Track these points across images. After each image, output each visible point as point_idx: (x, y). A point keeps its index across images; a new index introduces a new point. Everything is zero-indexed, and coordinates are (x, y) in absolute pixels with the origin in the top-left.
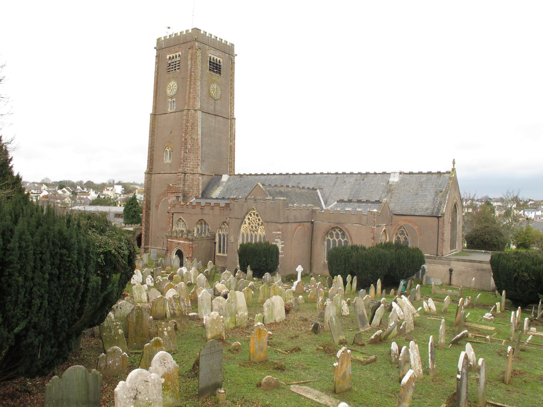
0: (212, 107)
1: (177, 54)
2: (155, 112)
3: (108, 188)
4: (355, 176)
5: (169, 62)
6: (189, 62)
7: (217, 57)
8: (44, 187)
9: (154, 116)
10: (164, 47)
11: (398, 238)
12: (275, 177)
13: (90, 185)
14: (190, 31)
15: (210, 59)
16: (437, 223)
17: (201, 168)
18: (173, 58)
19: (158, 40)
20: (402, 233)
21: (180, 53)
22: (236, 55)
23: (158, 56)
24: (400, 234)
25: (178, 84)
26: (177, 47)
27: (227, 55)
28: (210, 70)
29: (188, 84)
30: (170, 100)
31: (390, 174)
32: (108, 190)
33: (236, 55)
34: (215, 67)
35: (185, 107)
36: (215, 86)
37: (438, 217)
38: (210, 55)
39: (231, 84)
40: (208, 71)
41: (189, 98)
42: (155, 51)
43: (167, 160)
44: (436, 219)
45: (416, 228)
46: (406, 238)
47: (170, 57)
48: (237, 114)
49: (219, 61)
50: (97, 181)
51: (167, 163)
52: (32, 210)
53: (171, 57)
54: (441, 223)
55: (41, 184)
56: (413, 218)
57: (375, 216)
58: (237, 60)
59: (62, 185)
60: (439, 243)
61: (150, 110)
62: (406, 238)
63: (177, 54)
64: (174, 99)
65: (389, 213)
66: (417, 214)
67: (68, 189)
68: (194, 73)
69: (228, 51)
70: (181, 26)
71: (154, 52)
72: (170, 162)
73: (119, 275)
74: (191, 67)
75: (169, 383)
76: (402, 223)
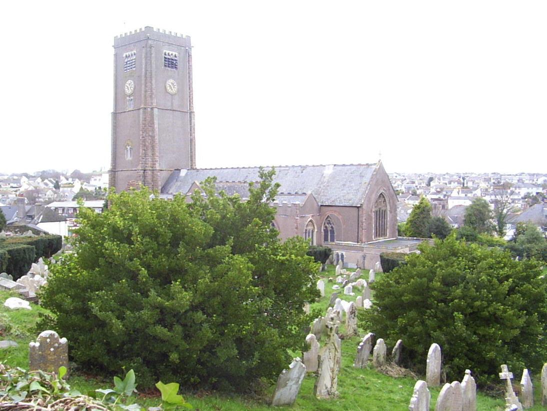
0: (170, 104)
1: (133, 52)
4: (355, 167)
5: (126, 61)
6: (144, 61)
7: (172, 53)
8: (24, 179)
9: (115, 115)
10: (121, 44)
11: (326, 227)
12: (226, 171)
13: (77, 175)
15: (165, 54)
16: (356, 214)
18: (129, 56)
20: (329, 223)
21: (135, 52)
22: (193, 47)
23: (116, 55)
24: (328, 223)
25: (134, 82)
26: (132, 46)
27: (183, 48)
28: (165, 66)
29: (143, 82)
31: (325, 166)
33: (193, 47)
34: (171, 63)
35: (141, 105)
39: (189, 77)
41: (145, 96)
42: (113, 49)
43: (129, 157)
44: (356, 208)
45: (340, 217)
46: (332, 227)
47: (126, 56)
48: (196, 108)
49: (175, 55)
51: (129, 160)
53: (128, 56)
54: (360, 213)
56: (338, 208)
57: (298, 208)
58: (194, 53)
59: (44, 176)
60: (359, 231)
61: (111, 109)
62: (332, 227)
63: (133, 52)
64: (132, 98)
66: (341, 205)
68: (152, 71)
69: (184, 45)
71: (112, 51)
72: (131, 159)
73: (504, 367)
75: (250, 381)
76: (328, 214)
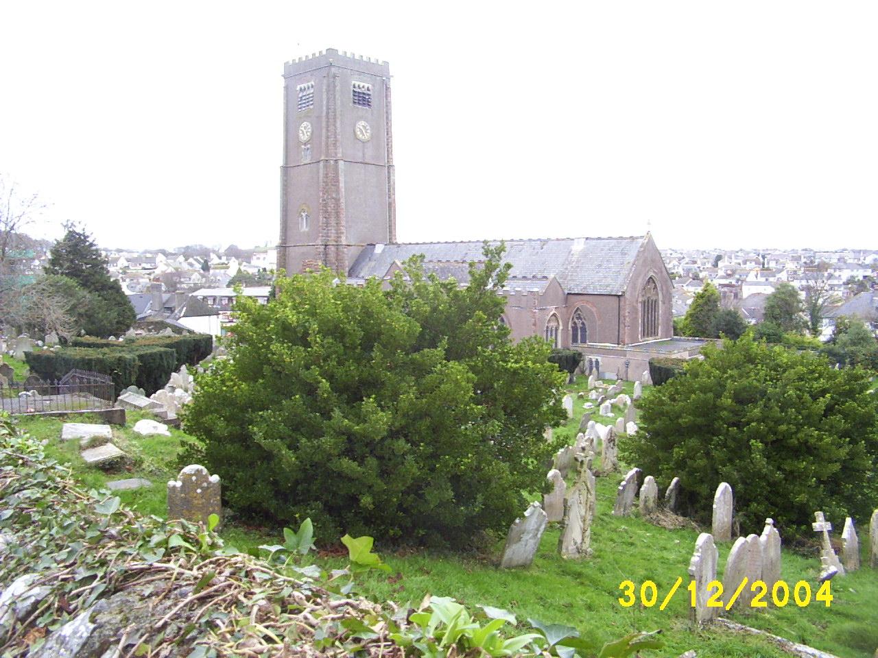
0: (360, 154)
2: (286, 163)
3: (258, 256)
6: (325, 96)
7: (364, 84)
8: (161, 257)
9: (286, 169)
10: (294, 73)
11: (575, 323)
13: (233, 252)
14: (324, 53)
17: (346, 237)
19: (286, 64)
20: (579, 318)
21: (313, 83)
23: (286, 88)
26: (309, 75)
27: (378, 78)
28: (354, 103)
29: (324, 124)
30: (303, 146)
31: (573, 240)
32: (258, 258)
34: (362, 99)
35: (321, 156)
36: (361, 124)
37: (619, 296)
38: (353, 82)
40: (351, 104)
43: (304, 228)
45: (594, 310)
46: (583, 323)
48: (397, 160)
50: (244, 246)
51: (304, 232)
52: (126, 365)
54: (622, 303)
55: (157, 252)
61: (280, 162)
62: (583, 323)
63: (310, 84)
64: (309, 146)
65: (561, 292)
67: (196, 260)
70: (310, 47)
71: (281, 83)
72: (307, 230)
74: (328, 102)
76: (578, 305)
